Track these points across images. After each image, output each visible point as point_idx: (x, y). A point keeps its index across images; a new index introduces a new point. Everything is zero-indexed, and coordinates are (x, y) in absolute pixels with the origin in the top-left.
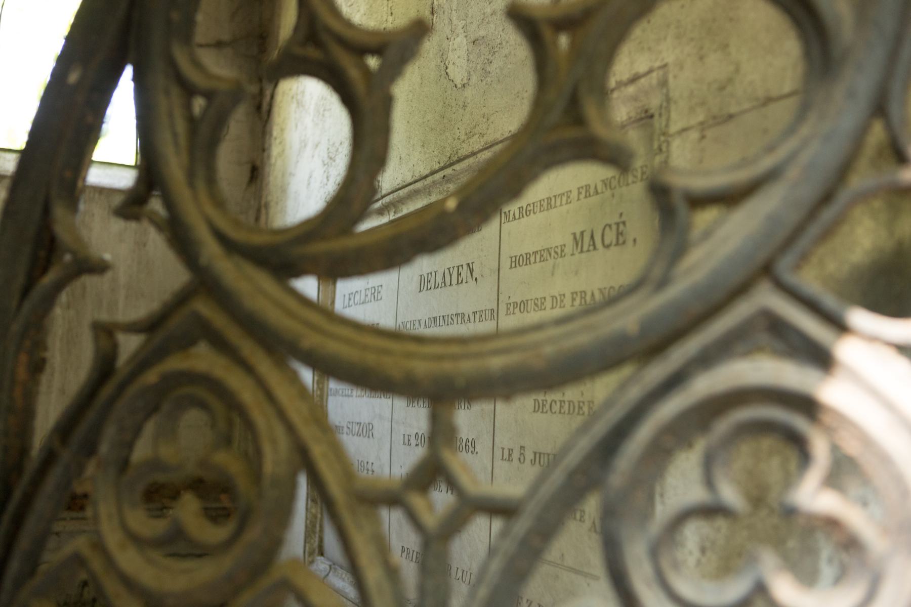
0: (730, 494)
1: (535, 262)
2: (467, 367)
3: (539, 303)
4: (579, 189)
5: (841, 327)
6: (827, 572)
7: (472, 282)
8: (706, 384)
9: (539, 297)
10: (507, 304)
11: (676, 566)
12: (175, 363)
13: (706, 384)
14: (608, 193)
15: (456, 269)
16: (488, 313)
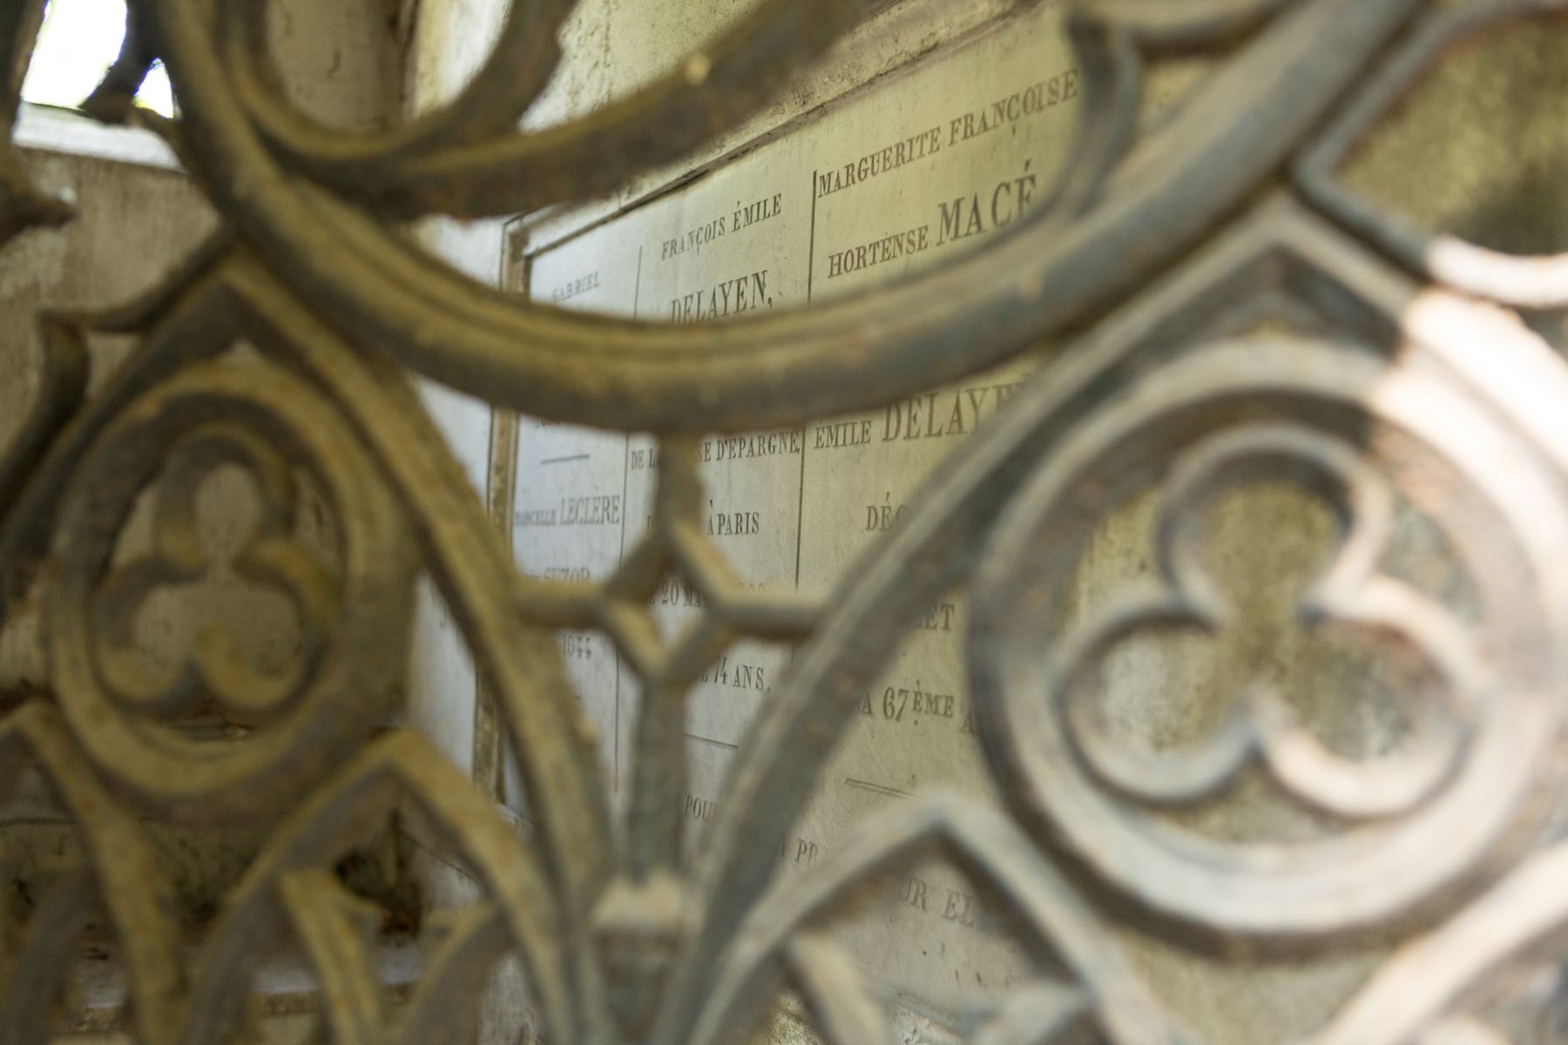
0: (1201, 589)
1: (874, 262)
2: (723, 368)
4: (953, 123)
5: (1419, 277)
6: (1376, 736)
8: (1161, 389)
11: (1100, 723)
12: (191, 381)
13: (1161, 389)
14: (1006, 125)
15: (735, 285)
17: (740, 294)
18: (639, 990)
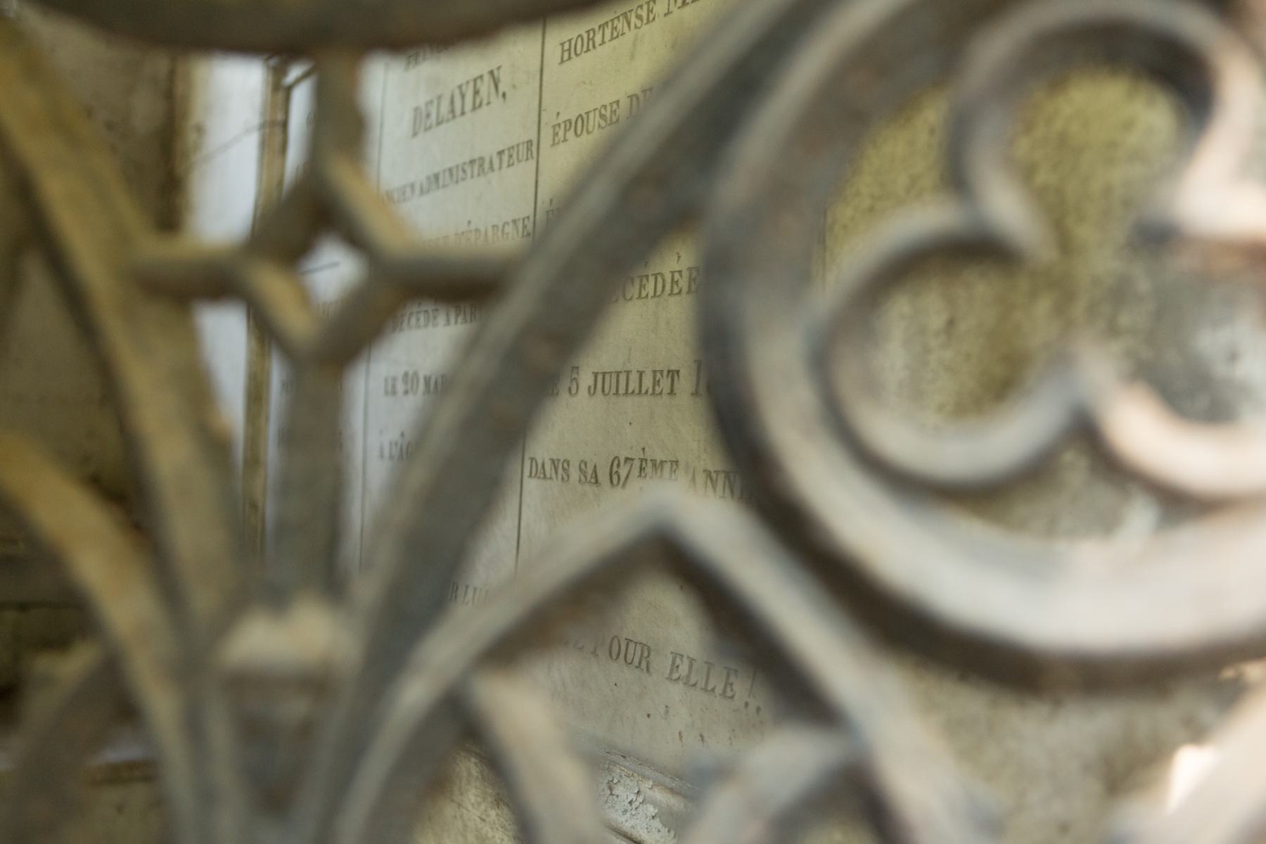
0: (1006, 207)
3: (608, 114)
7: (497, 101)
9: (606, 102)
10: (554, 127)
11: (873, 388)
15: (471, 84)
16: (523, 149)
17: (476, 92)
18: (284, 746)
